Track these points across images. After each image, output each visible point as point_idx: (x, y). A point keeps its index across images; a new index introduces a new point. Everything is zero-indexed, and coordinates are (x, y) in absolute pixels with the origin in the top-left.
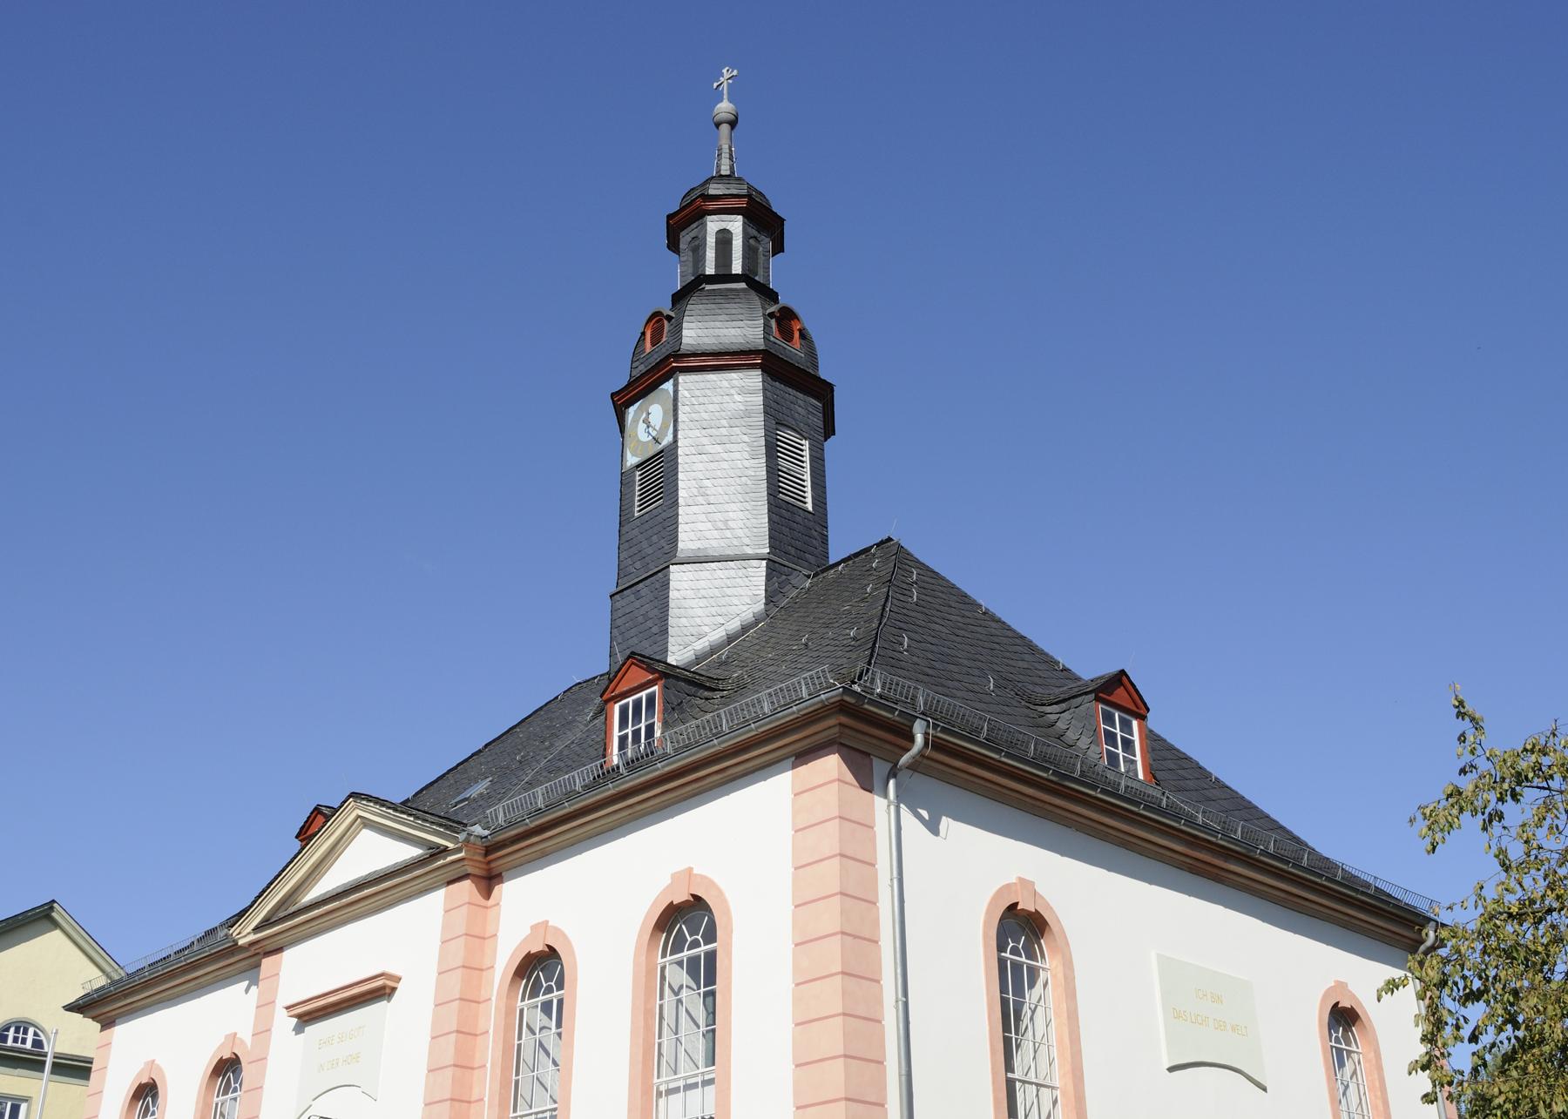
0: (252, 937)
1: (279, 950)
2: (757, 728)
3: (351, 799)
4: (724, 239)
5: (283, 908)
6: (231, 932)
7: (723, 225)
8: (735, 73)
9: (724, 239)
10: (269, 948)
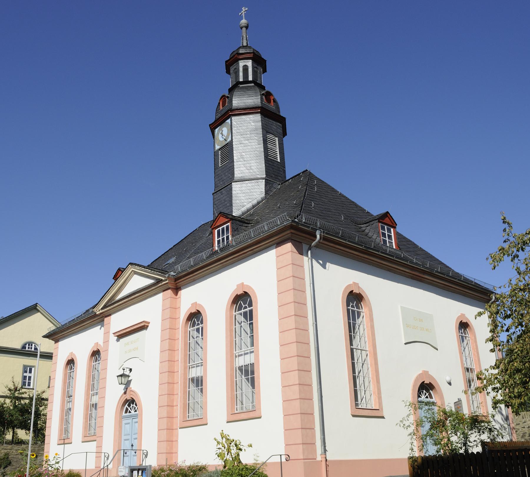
0: (101, 311)
1: (110, 315)
2: (263, 235)
3: (130, 265)
4: (246, 68)
5: (110, 301)
6: (94, 310)
7: (245, 64)
8: (247, 9)
9: (246, 68)
10: (106, 315)
